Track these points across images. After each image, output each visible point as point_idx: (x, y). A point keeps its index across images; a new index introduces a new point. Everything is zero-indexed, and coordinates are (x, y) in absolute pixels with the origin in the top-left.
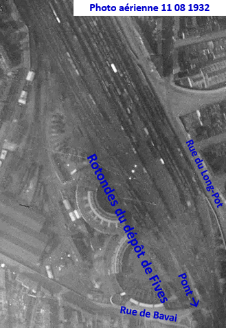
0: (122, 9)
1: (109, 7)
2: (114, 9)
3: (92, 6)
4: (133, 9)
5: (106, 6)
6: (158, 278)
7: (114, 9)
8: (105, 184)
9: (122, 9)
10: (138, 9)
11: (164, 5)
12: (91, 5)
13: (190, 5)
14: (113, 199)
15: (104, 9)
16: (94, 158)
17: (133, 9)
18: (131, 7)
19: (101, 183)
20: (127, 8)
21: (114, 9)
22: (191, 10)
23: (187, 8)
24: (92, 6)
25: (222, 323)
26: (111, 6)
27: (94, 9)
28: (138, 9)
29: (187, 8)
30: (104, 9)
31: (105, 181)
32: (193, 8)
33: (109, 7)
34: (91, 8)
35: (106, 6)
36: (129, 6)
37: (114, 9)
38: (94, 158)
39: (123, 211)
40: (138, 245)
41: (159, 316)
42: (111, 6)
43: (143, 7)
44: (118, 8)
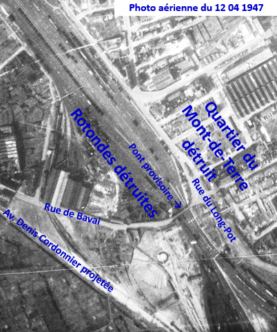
0: (161, 9)
1: (148, 7)
2: (153, 9)
3: (131, 6)
4: (173, 9)
5: (146, 6)
6: (108, 161)
7: (153, 9)
8: (204, 169)
9: (161, 9)
10: (178, 9)
11: (217, 5)
12: (131, 5)
13: (244, 5)
14: (109, 157)
15: (144, 9)
16: (79, 113)
17: (173, 9)
18: (171, 7)
19: (230, 140)
20: (166, 9)
21: (153, 9)
22: (244, 10)
23: (241, 8)
24: (131, 6)
25: (274, 328)
26: (150, 6)
27: (133, 9)
28: (178, 9)
29: (241, 8)
30: (144, 9)
31: (220, 217)
32: (247, 8)
33: (148, 7)
34: (131, 8)
35: (146, 6)
36: (169, 6)
37: (153, 9)
38: (79, 113)
39: (123, 167)
40: (101, 143)
41: (83, 217)
42: (150, 6)
43: (183, 7)
44: (157, 8)
